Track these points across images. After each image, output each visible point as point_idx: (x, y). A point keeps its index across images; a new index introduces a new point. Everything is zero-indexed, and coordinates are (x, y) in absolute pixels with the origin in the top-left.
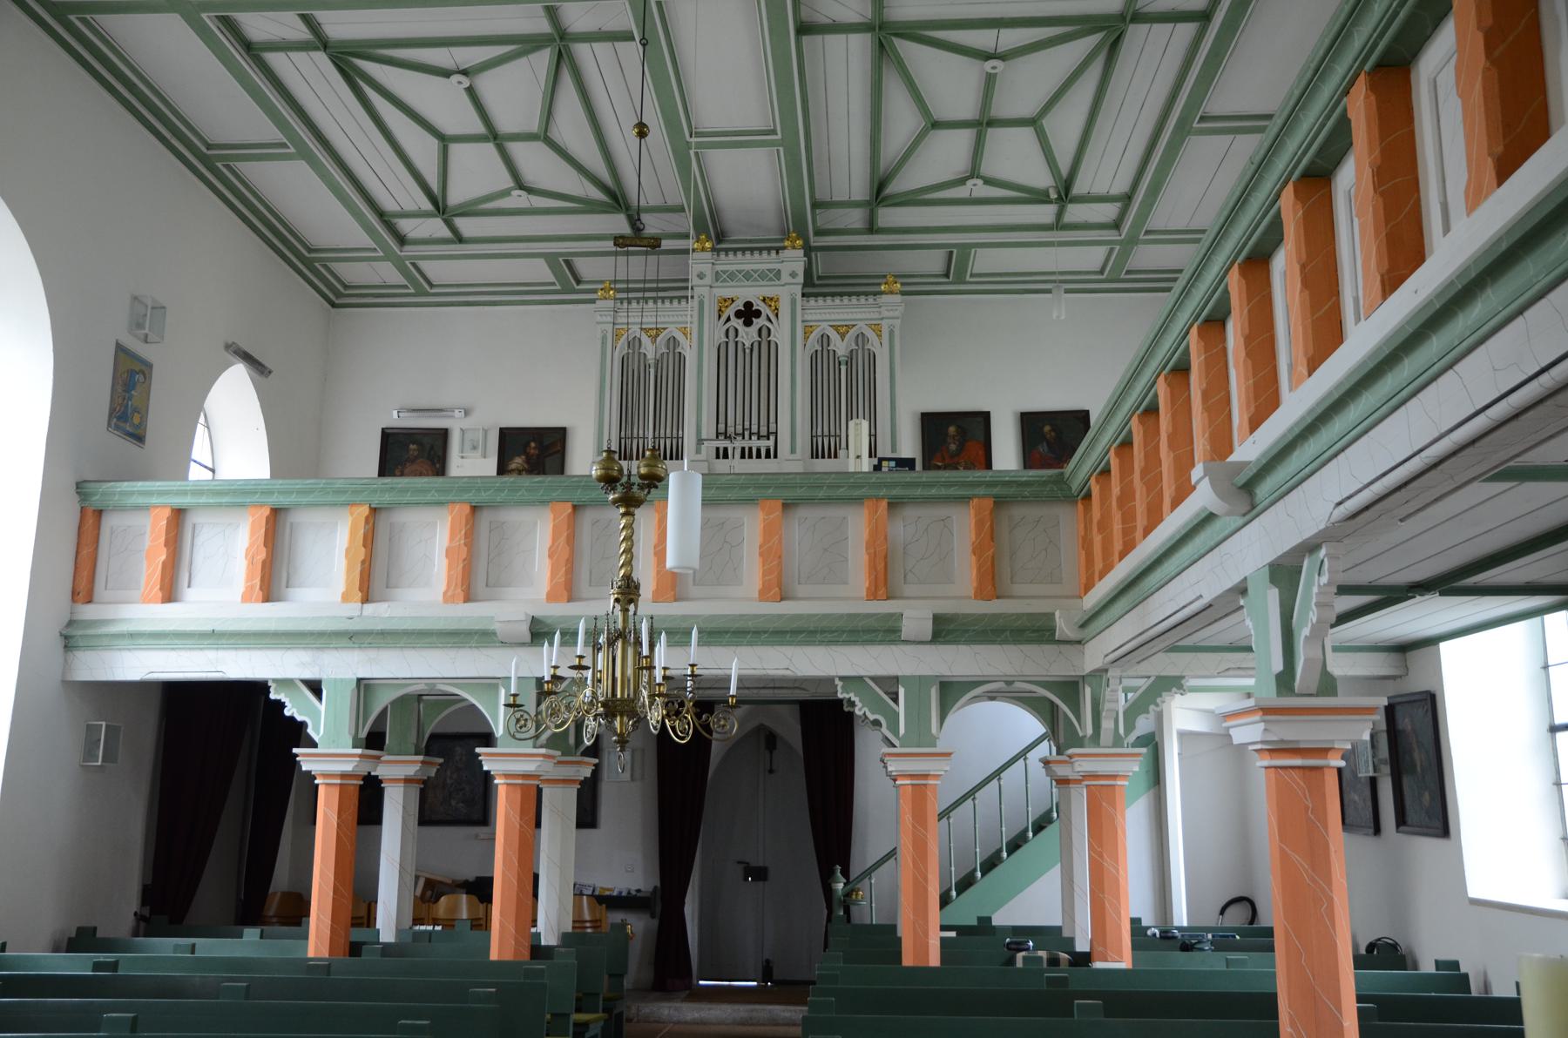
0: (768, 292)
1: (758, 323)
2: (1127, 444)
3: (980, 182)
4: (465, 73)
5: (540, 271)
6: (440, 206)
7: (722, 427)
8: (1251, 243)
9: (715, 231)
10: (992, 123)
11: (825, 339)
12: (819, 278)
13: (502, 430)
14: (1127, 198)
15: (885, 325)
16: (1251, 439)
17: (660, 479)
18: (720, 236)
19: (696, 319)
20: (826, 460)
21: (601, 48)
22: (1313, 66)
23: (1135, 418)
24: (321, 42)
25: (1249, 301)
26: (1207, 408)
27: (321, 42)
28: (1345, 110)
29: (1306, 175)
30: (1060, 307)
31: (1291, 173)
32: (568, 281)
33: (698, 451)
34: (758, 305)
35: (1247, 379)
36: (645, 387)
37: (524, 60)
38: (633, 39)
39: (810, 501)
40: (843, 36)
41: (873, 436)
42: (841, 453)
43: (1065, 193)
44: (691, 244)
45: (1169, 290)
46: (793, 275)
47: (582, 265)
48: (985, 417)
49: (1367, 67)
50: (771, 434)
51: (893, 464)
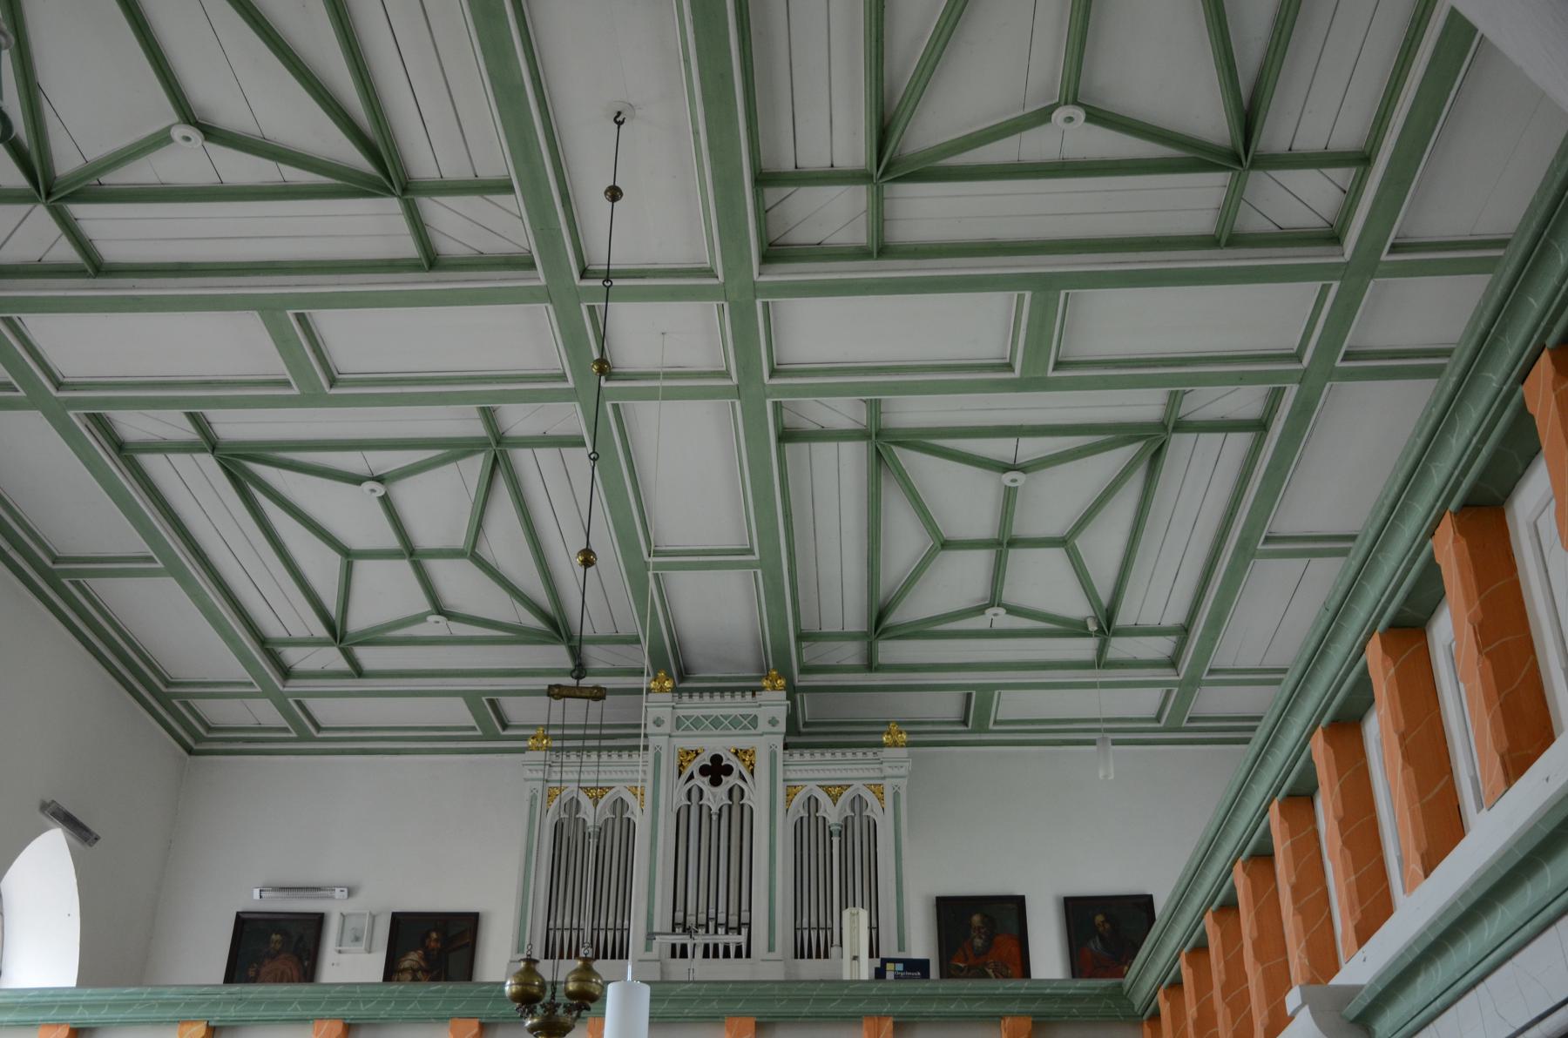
0: (743, 743)
1: (729, 781)
2: (1201, 948)
3: (1002, 611)
4: (380, 479)
5: (457, 713)
6: (337, 633)
7: (679, 915)
8: (1335, 703)
9: (677, 667)
10: (1014, 543)
11: (812, 803)
12: (806, 724)
13: (395, 915)
14: (1184, 631)
15: (888, 784)
16: (1360, 954)
17: (593, 998)
18: (684, 673)
19: (650, 777)
20: (814, 961)
21: (546, 455)
22: (1388, 502)
23: (1209, 916)
24: (210, 443)
25: (1340, 775)
26: (1300, 910)
27: (210, 443)
28: (1432, 554)
29: (1394, 625)
30: (1106, 765)
31: (1376, 623)
32: (492, 725)
33: (648, 948)
34: (729, 759)
35: (1347, 876)
36: (581, 861)
37: (451, 467)
38: (583, 444)
39: (792, 1020)
40: (833, 445)
41: (874, 929)
42: (834, 951)
43: (1107, 624)
44: (644, 682)
45: (1246, 741)
46: (773, 722)
47: (510, 706)
48: (1019, 902)
49: (1453, 506)
50: (744, 925)
51: (900, 967)
